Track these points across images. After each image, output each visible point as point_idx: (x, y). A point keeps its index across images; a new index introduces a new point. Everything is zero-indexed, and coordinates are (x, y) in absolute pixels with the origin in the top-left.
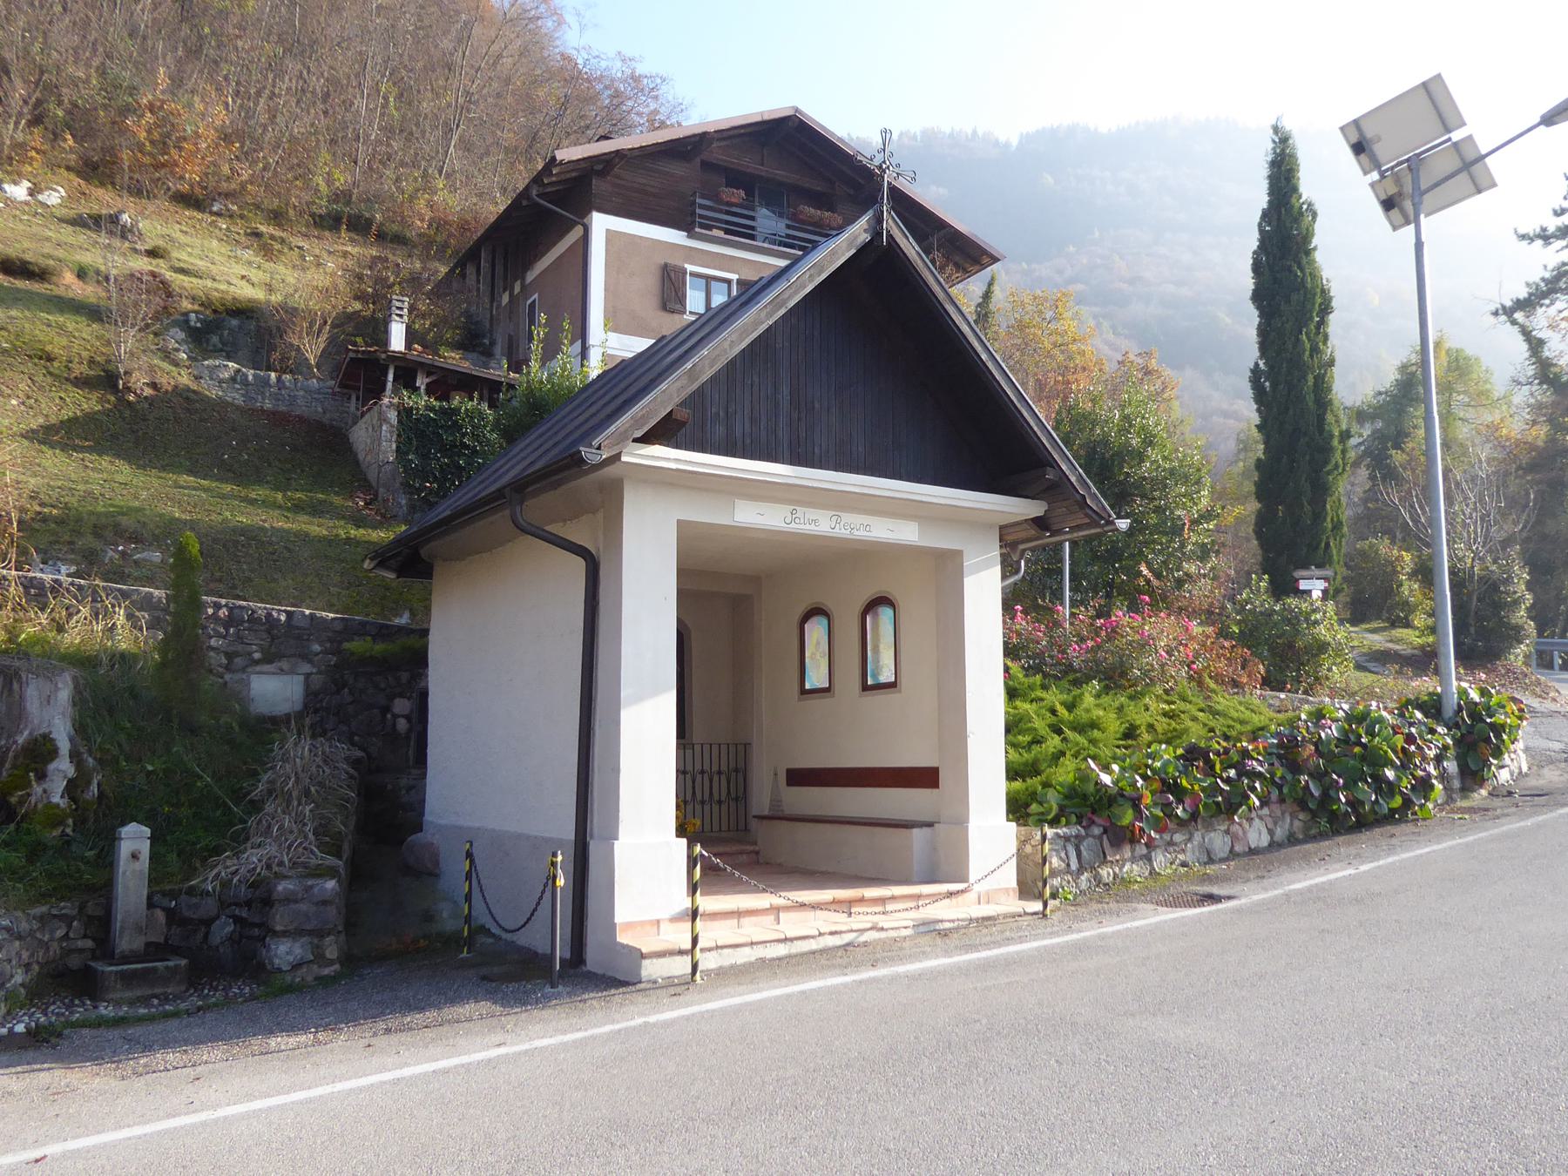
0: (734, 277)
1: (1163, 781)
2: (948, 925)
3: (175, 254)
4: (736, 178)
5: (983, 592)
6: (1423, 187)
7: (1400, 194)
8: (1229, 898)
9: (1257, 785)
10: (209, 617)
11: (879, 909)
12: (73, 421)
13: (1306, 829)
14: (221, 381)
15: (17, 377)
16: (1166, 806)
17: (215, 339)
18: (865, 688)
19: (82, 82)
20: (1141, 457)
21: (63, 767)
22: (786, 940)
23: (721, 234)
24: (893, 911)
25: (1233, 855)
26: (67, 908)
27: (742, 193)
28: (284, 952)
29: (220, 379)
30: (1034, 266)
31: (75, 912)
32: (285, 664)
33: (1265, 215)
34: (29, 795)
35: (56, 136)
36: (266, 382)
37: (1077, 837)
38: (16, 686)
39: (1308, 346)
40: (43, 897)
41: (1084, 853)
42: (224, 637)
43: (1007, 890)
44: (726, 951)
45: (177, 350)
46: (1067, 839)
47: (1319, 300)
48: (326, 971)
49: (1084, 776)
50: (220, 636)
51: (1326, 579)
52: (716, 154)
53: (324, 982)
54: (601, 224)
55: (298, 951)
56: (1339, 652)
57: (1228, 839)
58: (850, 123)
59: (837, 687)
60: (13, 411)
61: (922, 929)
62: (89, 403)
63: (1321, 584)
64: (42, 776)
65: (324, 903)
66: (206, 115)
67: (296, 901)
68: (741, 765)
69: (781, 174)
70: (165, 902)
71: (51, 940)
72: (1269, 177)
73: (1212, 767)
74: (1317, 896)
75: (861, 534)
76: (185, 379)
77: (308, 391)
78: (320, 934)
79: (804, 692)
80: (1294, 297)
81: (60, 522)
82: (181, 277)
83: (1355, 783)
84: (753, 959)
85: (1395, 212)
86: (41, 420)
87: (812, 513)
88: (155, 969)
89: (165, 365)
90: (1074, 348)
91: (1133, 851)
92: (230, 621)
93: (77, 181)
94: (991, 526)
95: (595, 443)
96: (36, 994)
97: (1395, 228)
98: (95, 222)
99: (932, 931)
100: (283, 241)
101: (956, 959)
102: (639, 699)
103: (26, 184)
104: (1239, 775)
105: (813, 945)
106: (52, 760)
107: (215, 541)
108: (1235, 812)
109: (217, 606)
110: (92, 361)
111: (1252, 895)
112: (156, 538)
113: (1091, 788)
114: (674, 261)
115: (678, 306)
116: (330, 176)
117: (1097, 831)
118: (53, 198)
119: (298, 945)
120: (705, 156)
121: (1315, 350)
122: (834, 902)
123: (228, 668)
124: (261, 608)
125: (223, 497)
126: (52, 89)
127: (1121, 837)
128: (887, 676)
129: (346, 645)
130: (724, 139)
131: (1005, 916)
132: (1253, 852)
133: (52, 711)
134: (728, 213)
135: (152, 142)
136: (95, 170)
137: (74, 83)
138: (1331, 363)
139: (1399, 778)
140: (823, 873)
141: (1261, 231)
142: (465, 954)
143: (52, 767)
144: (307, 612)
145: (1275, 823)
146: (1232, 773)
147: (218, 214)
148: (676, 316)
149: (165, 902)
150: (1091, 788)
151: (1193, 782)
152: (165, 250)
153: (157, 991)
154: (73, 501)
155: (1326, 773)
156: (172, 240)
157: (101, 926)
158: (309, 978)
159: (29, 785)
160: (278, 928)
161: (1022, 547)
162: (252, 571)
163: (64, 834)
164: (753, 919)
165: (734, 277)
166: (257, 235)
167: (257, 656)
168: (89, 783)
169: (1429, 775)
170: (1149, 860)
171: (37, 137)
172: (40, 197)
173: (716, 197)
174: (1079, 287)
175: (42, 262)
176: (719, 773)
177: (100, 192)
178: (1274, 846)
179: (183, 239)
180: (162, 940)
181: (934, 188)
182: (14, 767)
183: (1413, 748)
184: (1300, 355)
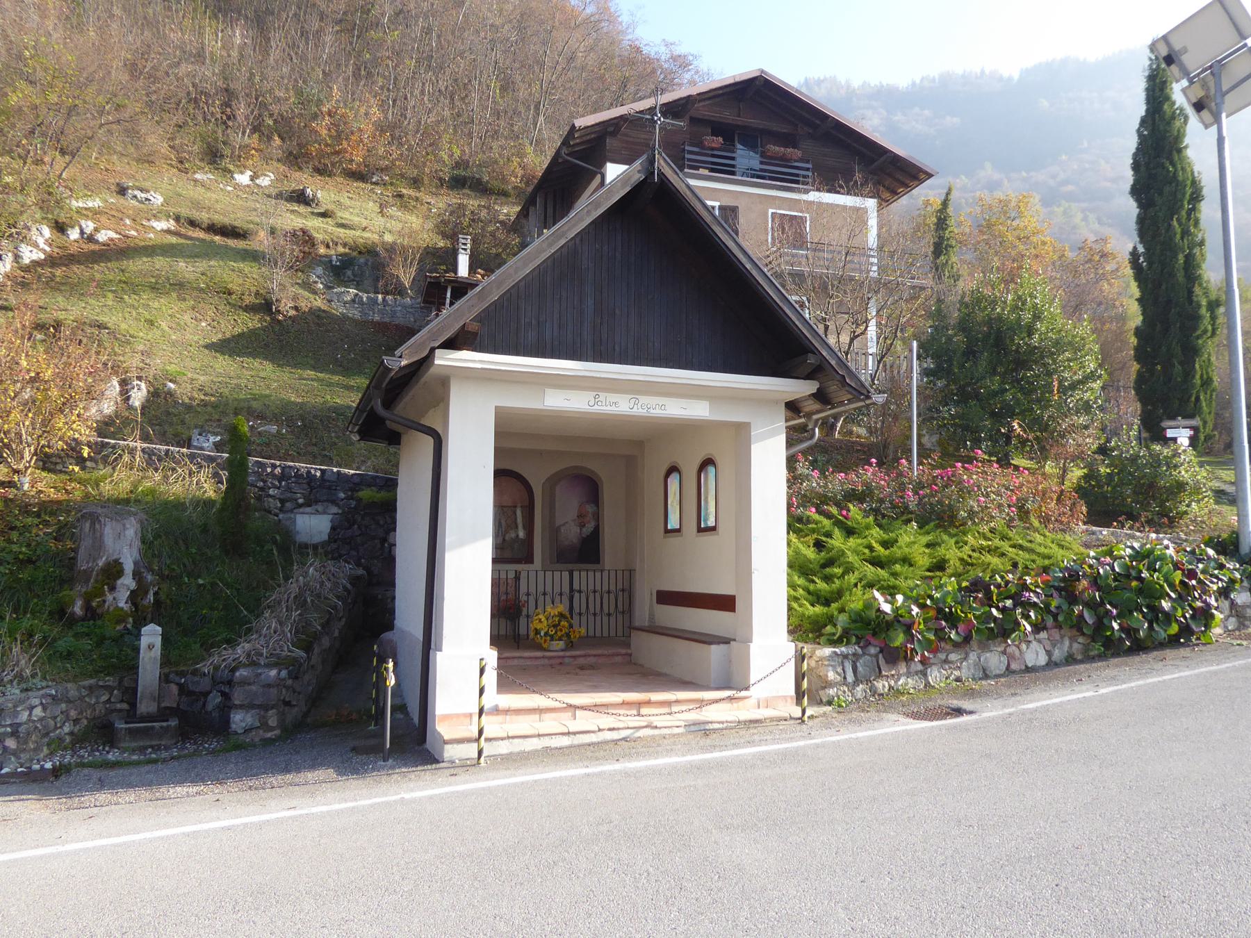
0: (717, 204)
1: (940, 611)
2: (716, 726)
3: (339, 214)
4: (718, 129)
5: (769, 461)
6: (1224, 89)
7: (1207, 96)
8: (971, 713)
9: (1032, 614)
11: (666, 710)
12: (241, 335)
13: (1086, 649)
14: (345, 303)
15: (207, 307)
16: (939, 632)
17: (349, 273)
18: (700, 530)
19: (284, 100)
20: (1030, 331)
21: (127, 582)
22: (569, 733)
23: (706, 172)
24: (668, 712)
25: (1009, 671)
26: (110, 681)
27: (720, 139)
28: (240, 720)
29: (344, 301)
30: (1033, 174)
31: (116, 684)
32: (320, 508)
33: (1143, 122)
34: (104, 601)
35: (270, 138)
36: (375, 301)
37: (854, 655)
38: (97, 526)
39: (1178, 230)
40: (96, 673)
41: (860, 669)
43: (785, 697)
44: (516, 740)
45: (316, 282)
46: (845, 657)
47: (1189, 191)
48: (269, 735)
49: (870, 604)
50: (275, 487)
51: (1191, 428)
52: (702, 111)
53: (267, 743)
56: (1197, 490)
57: (1004, 659)
58: (791, 74)
59: (684, 529)
60: (202, 330)
61: (693, 728)
62: (252, 322)
63: (1188, 432)
64: (113, 588)
65: (269, 686)
66: (366, 115)
67: (249, 684)
68: (626, 586)
70: (177, 679)
71: (97, 703)
72: (1147, 90)
73: (991, 599)
74: (1029, 719)
75: (657, 412)
76: (319, 303)
77: (404, 307)
78: (265, 708)
79: (667, 531)
80: (1167, 189)
81: (215, 406)
82: (342, 230)
83: (1131, 612)
84: (540, 747)
85: (1205, 113)
86: (220, 336)
87: (612, 397)
88: (153, 728)
89: (306, 294)
90: (1035, 239)
91: (908, 667)
92: (282, 477)
93: (282, 168)
94: (776, 402)
95: (398, 353)
96: (79, 740)
97: (1206, 127)
98: (300, 198)
99: (702, 730)
100: (417, 199)
102: (461, 543)
103: (249, 173)
104: (1015, 606)
107: (315, 417)
108: (1009, 637)
109: (274, 466)
110: (257, 293)
111: (990, 711)
112: (275, 415)
116: (450, 151)
117: (873, 650)
118: (264, 181)
120: (693, 113)
121: (1186, 233)
122: (624, 704)
123: (281, 510)
124: (302, 466)
125: (330, 385)
126: (264, 106)
127: (894, 656)
128: (711, 523)
129: (361, 494)
130: (709, 99)
131: (772, 719)
132: (1028, 670)
133: (123, 544)
135: (330, 136)
136: (295, 159)
137: (278, 100)
138: (1202, 243)
139: (1174, 609)
140: (665, 675)
141: (1140, 134)
142: (372, 727)
143: (119, 582)
144: (335, 470)
145: (1054, 646)
146: (1009, 603)
147: (376, 184)
149: (177, 679)
150: (873, 614)
151: (973, 612)
152: (332, 212)
153: (154, 743)
154: (226, 391)
155: (1102, 603)
156: (339, 203)
157: (131, 694)
158: (257, 739)
159: (103, 594)
160: (237, 702)
161: (815, 417)
162: (338, 437)
163: (126, 628)
164: (553, 715)
165: (717, 204)
166: (400, 196)
167: (301, 501)
168: (147, 593)
169: (1208, 605)
170: (925, 675)
171: (254, 140)
173: (700, 144)
174: (1070, 188)
175: (245, 226)
176: (609, 592)
177: (298, 174)
178: (1051, 664)
179: (348, 202)
181: (948, 118)
182: (96, 581)
183: (1194, 582)
184: (1171, 239)
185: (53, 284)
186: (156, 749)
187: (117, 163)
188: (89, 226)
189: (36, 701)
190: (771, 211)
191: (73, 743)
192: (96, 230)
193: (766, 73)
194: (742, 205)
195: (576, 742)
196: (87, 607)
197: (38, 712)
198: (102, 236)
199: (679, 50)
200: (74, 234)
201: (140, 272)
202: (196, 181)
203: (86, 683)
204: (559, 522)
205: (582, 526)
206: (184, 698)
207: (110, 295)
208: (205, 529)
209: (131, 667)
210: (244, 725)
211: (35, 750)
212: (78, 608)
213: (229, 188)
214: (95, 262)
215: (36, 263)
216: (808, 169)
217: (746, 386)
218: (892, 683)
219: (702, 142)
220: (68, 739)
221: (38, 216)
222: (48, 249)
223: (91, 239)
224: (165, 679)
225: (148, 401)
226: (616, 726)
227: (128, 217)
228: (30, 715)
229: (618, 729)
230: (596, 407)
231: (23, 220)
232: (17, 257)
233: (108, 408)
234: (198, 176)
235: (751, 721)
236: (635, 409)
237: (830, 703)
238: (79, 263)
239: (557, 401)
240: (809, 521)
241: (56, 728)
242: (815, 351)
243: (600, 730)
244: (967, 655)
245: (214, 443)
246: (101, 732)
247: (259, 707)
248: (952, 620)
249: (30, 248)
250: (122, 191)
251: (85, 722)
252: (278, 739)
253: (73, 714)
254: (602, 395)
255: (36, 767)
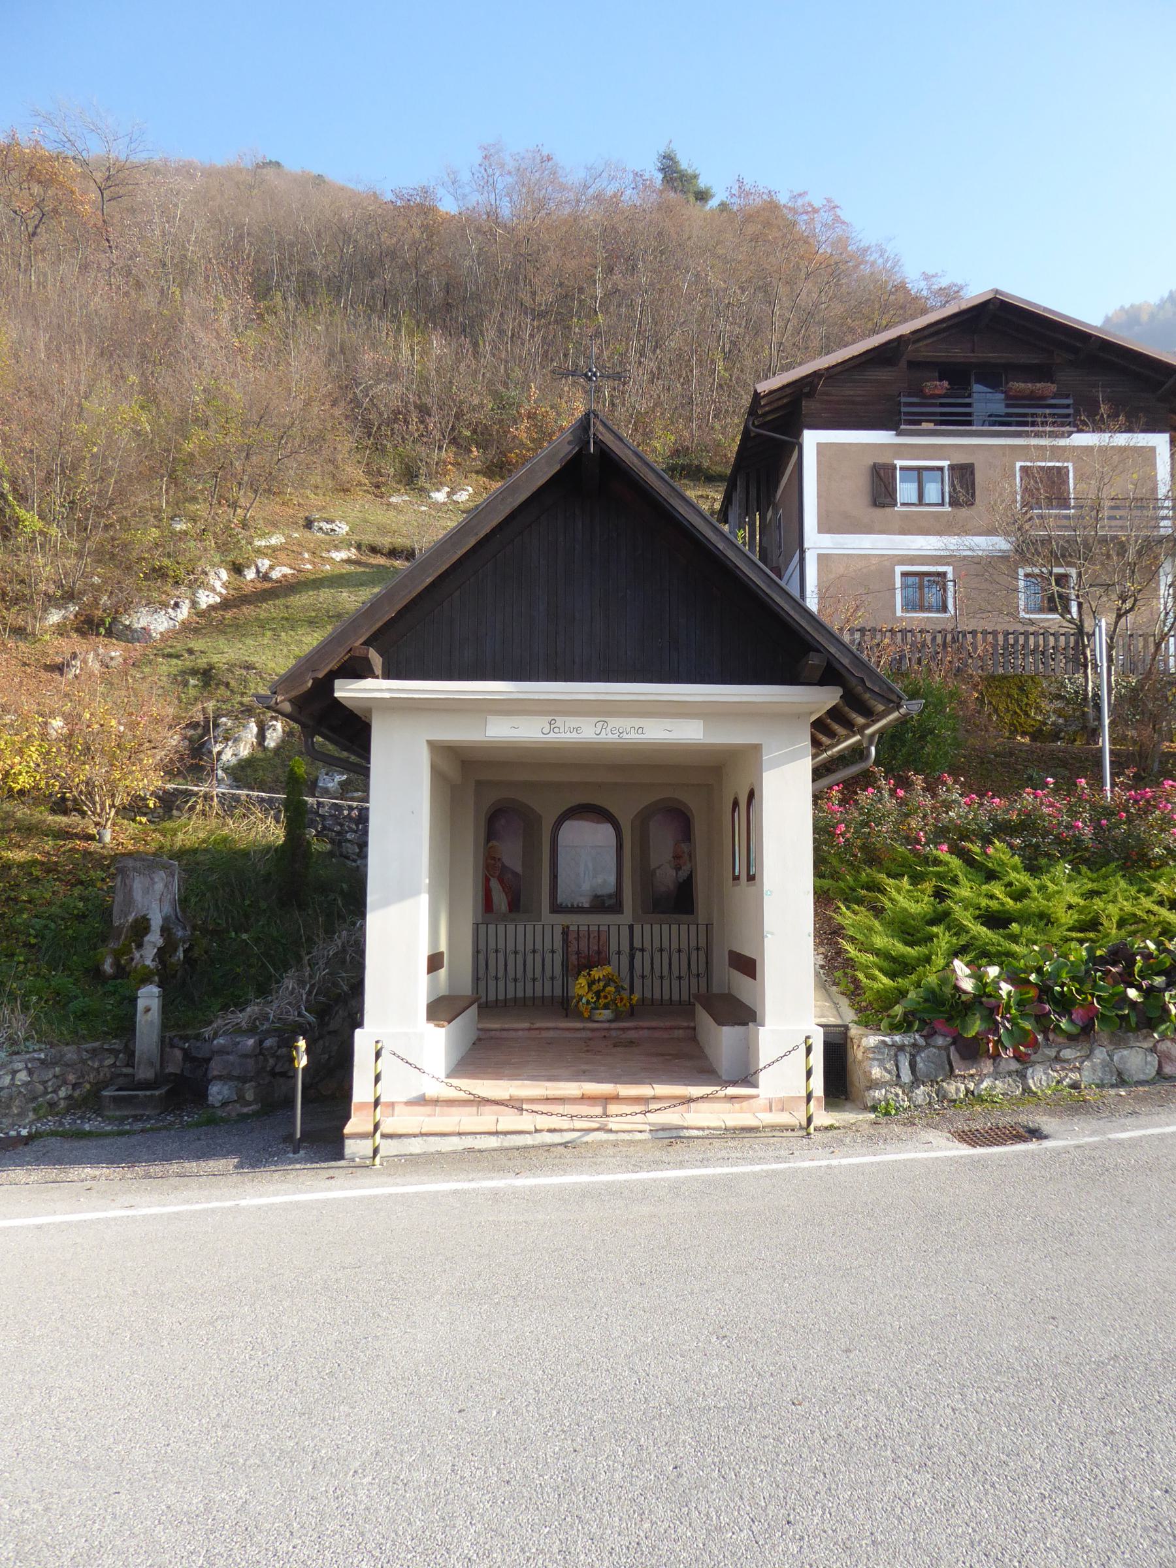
0: (945, 464)
10: (345, 817)
21: (154, 939)
23: (931, 426)
24: (707, 1110)
27: (946, 384)
28: (217, 1092)
34: (132, 959)
37: (914, 1045)
41: (920, 1065)
42: (356, 832)
46: (901, 1048)
48: (245, 1110)
52: (925, 352)
54: (811, 439)
55: (226, 1091)
57: (1153, 1059)
64: (140, 946)
65: (246, 1056)
67: (228, 1054)
69: (992, 356)
70: (181, 1044)
75: (632, 737)
87: (573, 722)
93: (483, 480)
94: (799, 716)
96: (75, 1105)
99: (671, 1136)
101: (643, 1175)
102: (385, 903)
105: (528, 1140)
106: (147, 934)
109: (351, 808)
111: (1068, 1137)
113: (948, 990)
114: (882, 460)
115: (888, 500)
117: (940, 1041)
118: (462, 497)
119: (226, 1087)
122: (584, 1099)
127: (972, 1051)
130: (925, 337)
133: (154, 900)
134: (942, 405)
146: (1159, 981)
148: (888, 510)
150: (948, 990)
158: (234, 1114)
159: (130, 952)
165: (945, 464)
168: (176, 949)
170: (1023, 1077)
171: (448, 454)
172: (455, 498)
180: (178, 1072)
185: (221, 627)
186: (137, 1118)
187: (312, 496)
188: (264, 564)
189: (21, 1066)
190: (1018, 464)
191: (67, 1110)
192: (272, 568)
193: (1002, 293)
194: (979, 461)
195: (506, 1144)
196: (117, 964)
197: (23, 1076)
198: (275, 575)
199: (944, 282)
200: (250, 574)
201: (303, 607)
202: (389, 504)
203: (88, 1046)
204: (654, 864)
205: (678, 868)
206: (188, 1065)
207: (269, 633)
208: (267, 878)
209: (126, 1026)
210: (220, 1098)
211: (19, 1115)
212: (108, 967)
213: (423, 508)
214: (265, 600)
215: (212, 608)
216: (1068, 406)
217: (745, 699)
218: (971, 1086)
219: (922, 391)
220: (62, 1104)
221: (217, 559)
222: (224, 592)
223: (266, 577)
224: (165, 1043)
225: (283, 741)
226: (557, 1127)
227: (308, 551)
228: (13, 1079)
229: (561, 1131)
230: (552, 735)
231: (203, 564)
232: (194, 604)
233: (245, 751)
234: (393, 500)
235: (744, 1129)
236: (603, 735)
237: (874, 1109)
238: (250, 603)
239: (502, 731)
240: (937, 862)
241: (46, 1093)
242: (818, 649)
243: (536, 1131)
244: (1092, 1051)
245: (340, 783)
246: (89, 1102)
247: (238, 1078)
248: (1064, 1004)
249: (207, 593)
250: (309, 524)
251: (88, 1086)
252: (255, 1114)
253: (71, 1078)
254: (560, 720)
255: (13, 1133)
